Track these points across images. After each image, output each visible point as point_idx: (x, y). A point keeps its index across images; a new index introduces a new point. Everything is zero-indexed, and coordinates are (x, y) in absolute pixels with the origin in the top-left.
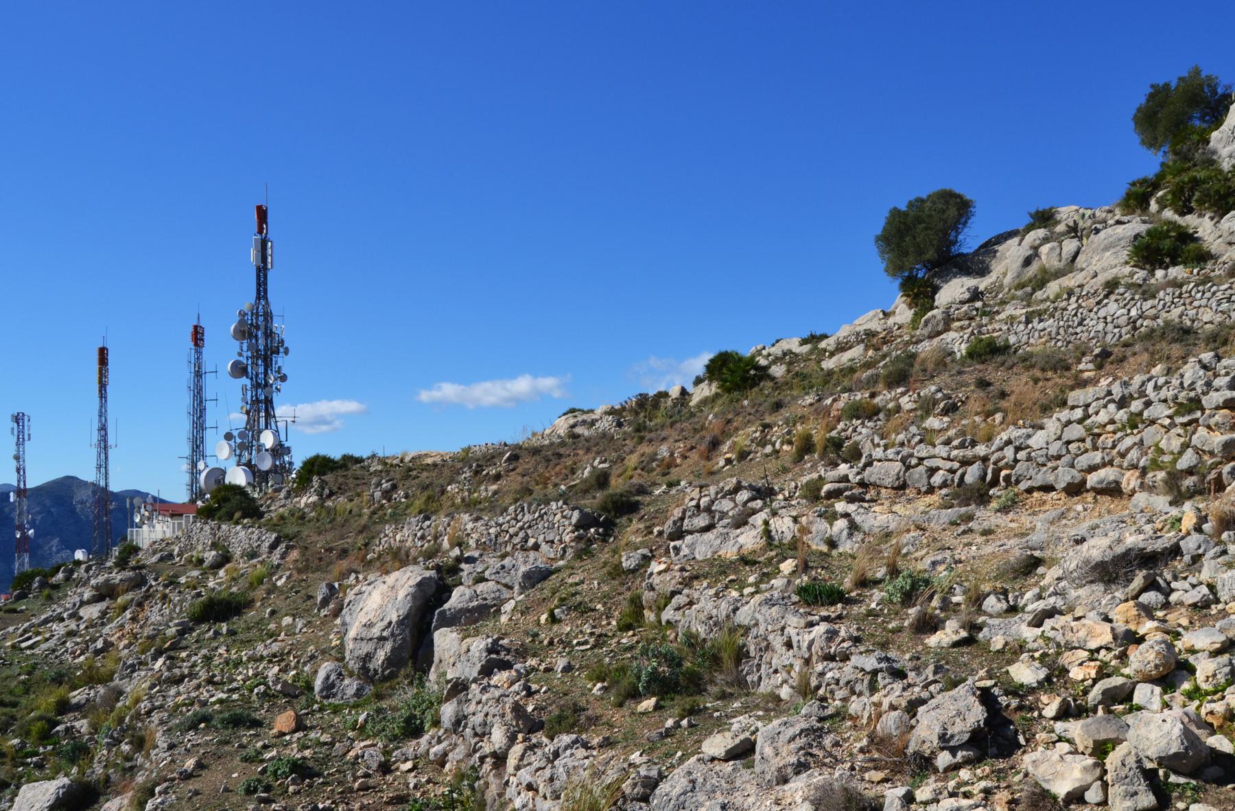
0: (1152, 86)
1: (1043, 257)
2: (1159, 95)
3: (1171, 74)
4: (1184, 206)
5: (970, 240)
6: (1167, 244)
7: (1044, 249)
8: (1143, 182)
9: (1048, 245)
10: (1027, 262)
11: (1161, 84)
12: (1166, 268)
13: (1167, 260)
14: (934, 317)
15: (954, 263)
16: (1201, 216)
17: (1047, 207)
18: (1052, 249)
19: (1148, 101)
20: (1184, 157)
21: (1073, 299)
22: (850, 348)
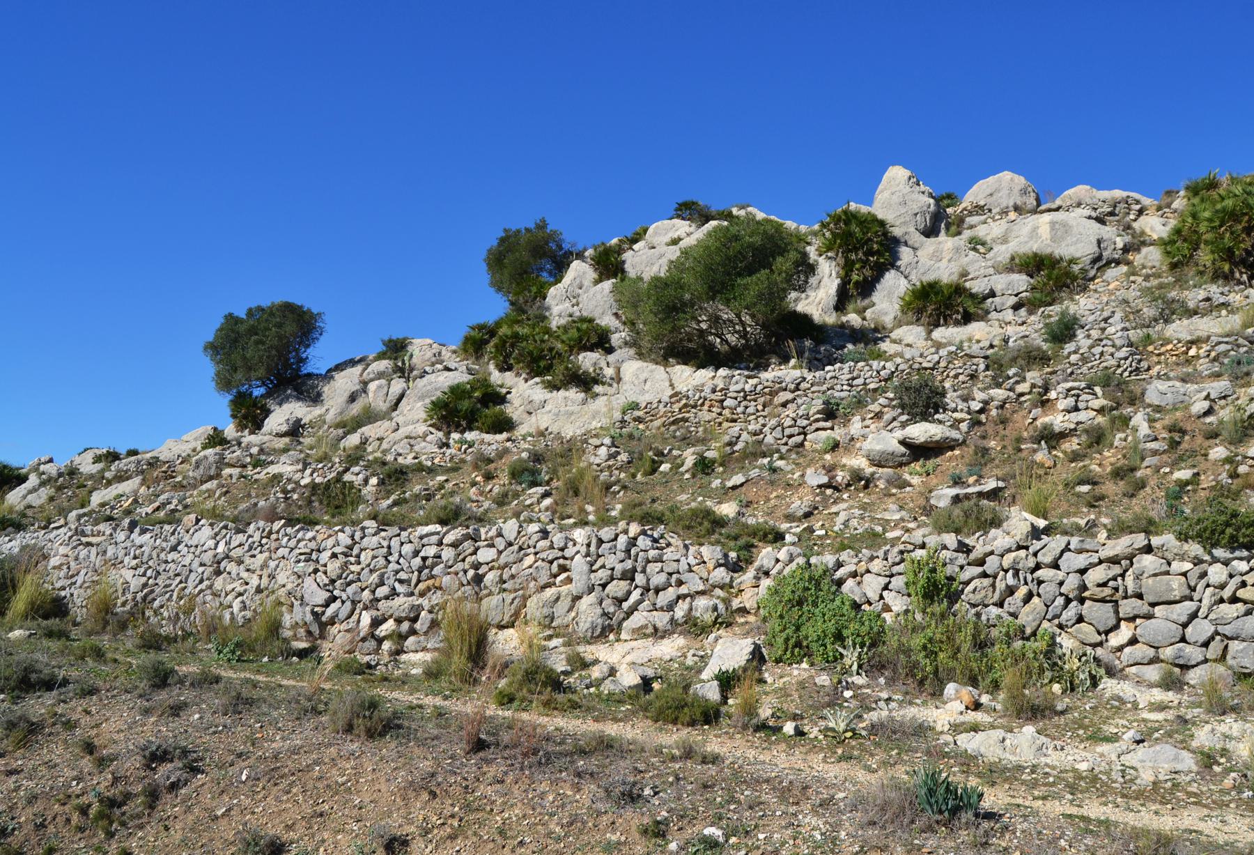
0: (505, 230)
1: (371, 395)
2: (508, 243)
3: (522, 220)
4: (505, 362)
5: (318, 357)
6: (465, 405)
7: (372, 386)
8: (481, 327)
9: (377, 382)
10: (353, 398)
11: (514, 229)
12: (462, 432)
13: (464, 423)
14: (206, 457)
15: (299, 384)
16: (518, 375)
17: (401, 337)
18: (380, 387)
19: (499, 245)
20: (518, 308)
21: (308, 471)
22: (128, 479)
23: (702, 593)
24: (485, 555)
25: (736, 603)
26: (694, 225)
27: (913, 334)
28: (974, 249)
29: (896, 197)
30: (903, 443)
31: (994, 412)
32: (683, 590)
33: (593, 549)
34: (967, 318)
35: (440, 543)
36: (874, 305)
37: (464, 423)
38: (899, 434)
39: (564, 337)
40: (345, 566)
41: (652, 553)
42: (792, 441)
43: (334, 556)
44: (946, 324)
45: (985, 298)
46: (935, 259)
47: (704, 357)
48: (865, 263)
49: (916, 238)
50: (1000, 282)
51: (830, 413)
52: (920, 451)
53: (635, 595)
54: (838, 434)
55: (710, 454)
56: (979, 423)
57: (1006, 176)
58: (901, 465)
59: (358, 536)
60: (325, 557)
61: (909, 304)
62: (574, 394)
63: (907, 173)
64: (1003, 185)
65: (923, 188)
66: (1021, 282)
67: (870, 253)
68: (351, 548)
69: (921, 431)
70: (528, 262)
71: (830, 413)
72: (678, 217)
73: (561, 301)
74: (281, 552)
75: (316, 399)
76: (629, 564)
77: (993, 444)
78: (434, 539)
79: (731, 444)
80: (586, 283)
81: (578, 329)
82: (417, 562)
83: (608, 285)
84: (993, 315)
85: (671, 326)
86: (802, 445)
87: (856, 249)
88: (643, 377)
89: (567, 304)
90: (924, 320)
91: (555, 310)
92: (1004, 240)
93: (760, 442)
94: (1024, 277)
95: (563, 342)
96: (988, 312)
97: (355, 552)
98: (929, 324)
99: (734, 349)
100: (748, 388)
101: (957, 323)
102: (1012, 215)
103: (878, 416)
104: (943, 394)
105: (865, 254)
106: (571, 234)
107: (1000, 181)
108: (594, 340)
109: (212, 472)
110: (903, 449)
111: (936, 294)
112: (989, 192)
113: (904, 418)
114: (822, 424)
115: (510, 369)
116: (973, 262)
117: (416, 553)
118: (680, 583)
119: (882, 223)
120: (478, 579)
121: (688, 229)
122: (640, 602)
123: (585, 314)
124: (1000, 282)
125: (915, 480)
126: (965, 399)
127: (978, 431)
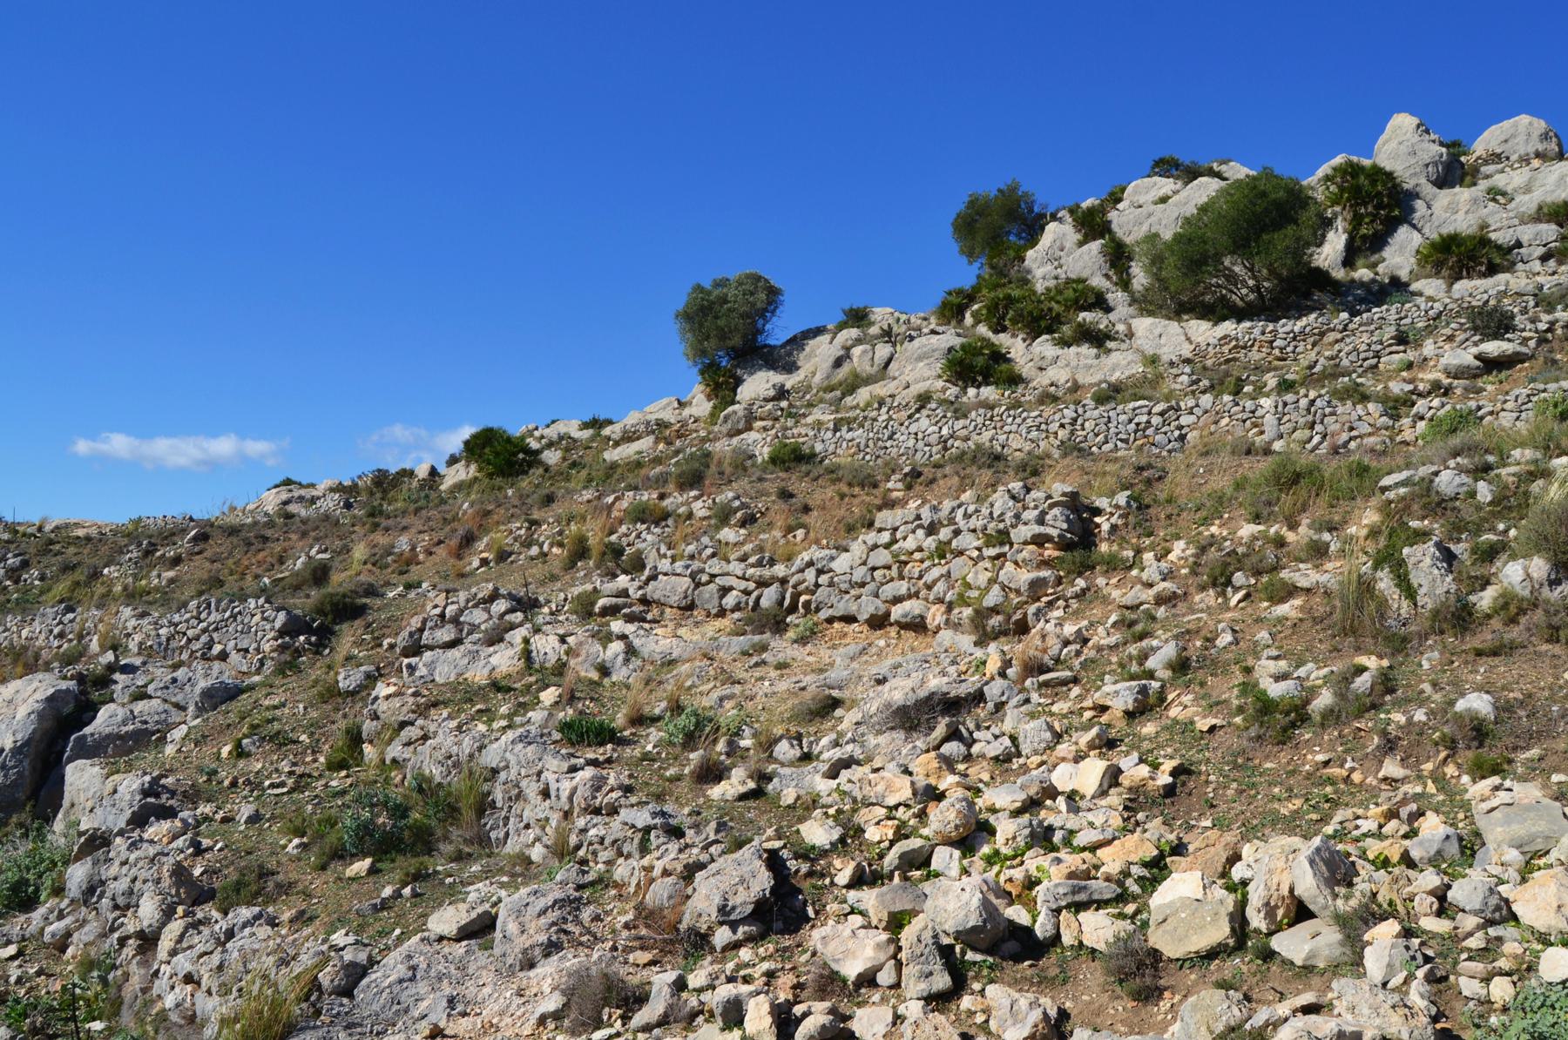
1: (855, 360)
3: (989, 186)
4: (999, 323)
5: (778, 331)
7: (856, 351)
8: (959, 292)
10: (838, 363)
12: (978, 387)
13: (980, 378)
14: (735, 412)
16: (1014, 336)
17: (862, 306)
18: (865, 352)
20: (1000, 272)
21: (884, 410)
23: (1370, 434)
24: (1185, 420)
25: (1398, 439)
26: (1180, 183)
27: (1431, 286)
28: (1494, 200)
29: (1401, 146)
30: (1476, 357)
31: (1559, 331)
32: (1354, 433)
33: (1280, 409)
34: (1492, 270)
35: (1149, 413)
36: (1384, 260)
37: (980, 378)
38: (1475, 350)
39: (1059, 298)
40: (1072, 433)
41: (1328, 410)
42: (1366, 364)
43: (1062, 426)
44: (1469, 277)
45: (1510, 249)
46: (1452, 212)
47: (1215, 311)
48: (1375, 217)
49: (1428, 189)
50: (1526, 233)
51: (1402, 339)
52: (1491, 365)
53: (1317, 439)
54: (1411, 355)
55: (1290, 377)
56: (1546, 341)
57: (1524, 119)
58: (1475, 376)
59: (1080, 411)
60: (1054, 427)
61: (1426, 257)
62: (1087, 351)
63: (1415, 121)
64: (1519, 131)
65: (1433, 137)
66: (1550, 231)
67: (1379, 207)
68: (1075, 420)
69: (1493, 348)
70: (1000, 226)
71: (1402, 339)
72: (1156, 174)
73: (1042, 264)
74: (1007, 428)
75: (791, 368)
76: (1310, 418)
77: (1559, 357)
78: (1145, 410)
79: (1311, 367)
80: (1068, 245)
81: (1075, 290)
82: (1132, 426)
83: (1095, 246)
84: (1520, 266)
85: (1190, 278)
86: (1376, 366)
87: (1365, 204)
88: (1157, 332)
89: (1049, 267)
90: (1445, 272)
91: (1039, 272)
92: (1528, 189)
93: (1337, 366)
94: (1554, 227)
95: (1058, 302)
96: (1514, 264)
97: (1080, 421)
98: (1450, 276)
99: (1249, 304)
100: (1297, 329)
101: (1484, 275)
102: (1536, 163)
103: (1450, 338)
104: (1513, 317)
105: (1375, 207)
106: (1043, 196)
107: (1516, 125)
108: (1091, 300)
109: (741, 426)
110: (1478, 363)
111: (1459, 246)
112: (1503, 138)
113: (1477, 338)
114: (1394, 348)
115: (1004, 329)
116: (1493, 213)
117: (1130, 421)
118: (1352, 429)
119: (1390, 175)
120: (1182, 438)
121: (1173, 187)
122: (1320, 443)
123: (1073, 276)
124: (1526, 233)
125: (1490, 388)
126: (1533, 321)
127: (1546, 347)
